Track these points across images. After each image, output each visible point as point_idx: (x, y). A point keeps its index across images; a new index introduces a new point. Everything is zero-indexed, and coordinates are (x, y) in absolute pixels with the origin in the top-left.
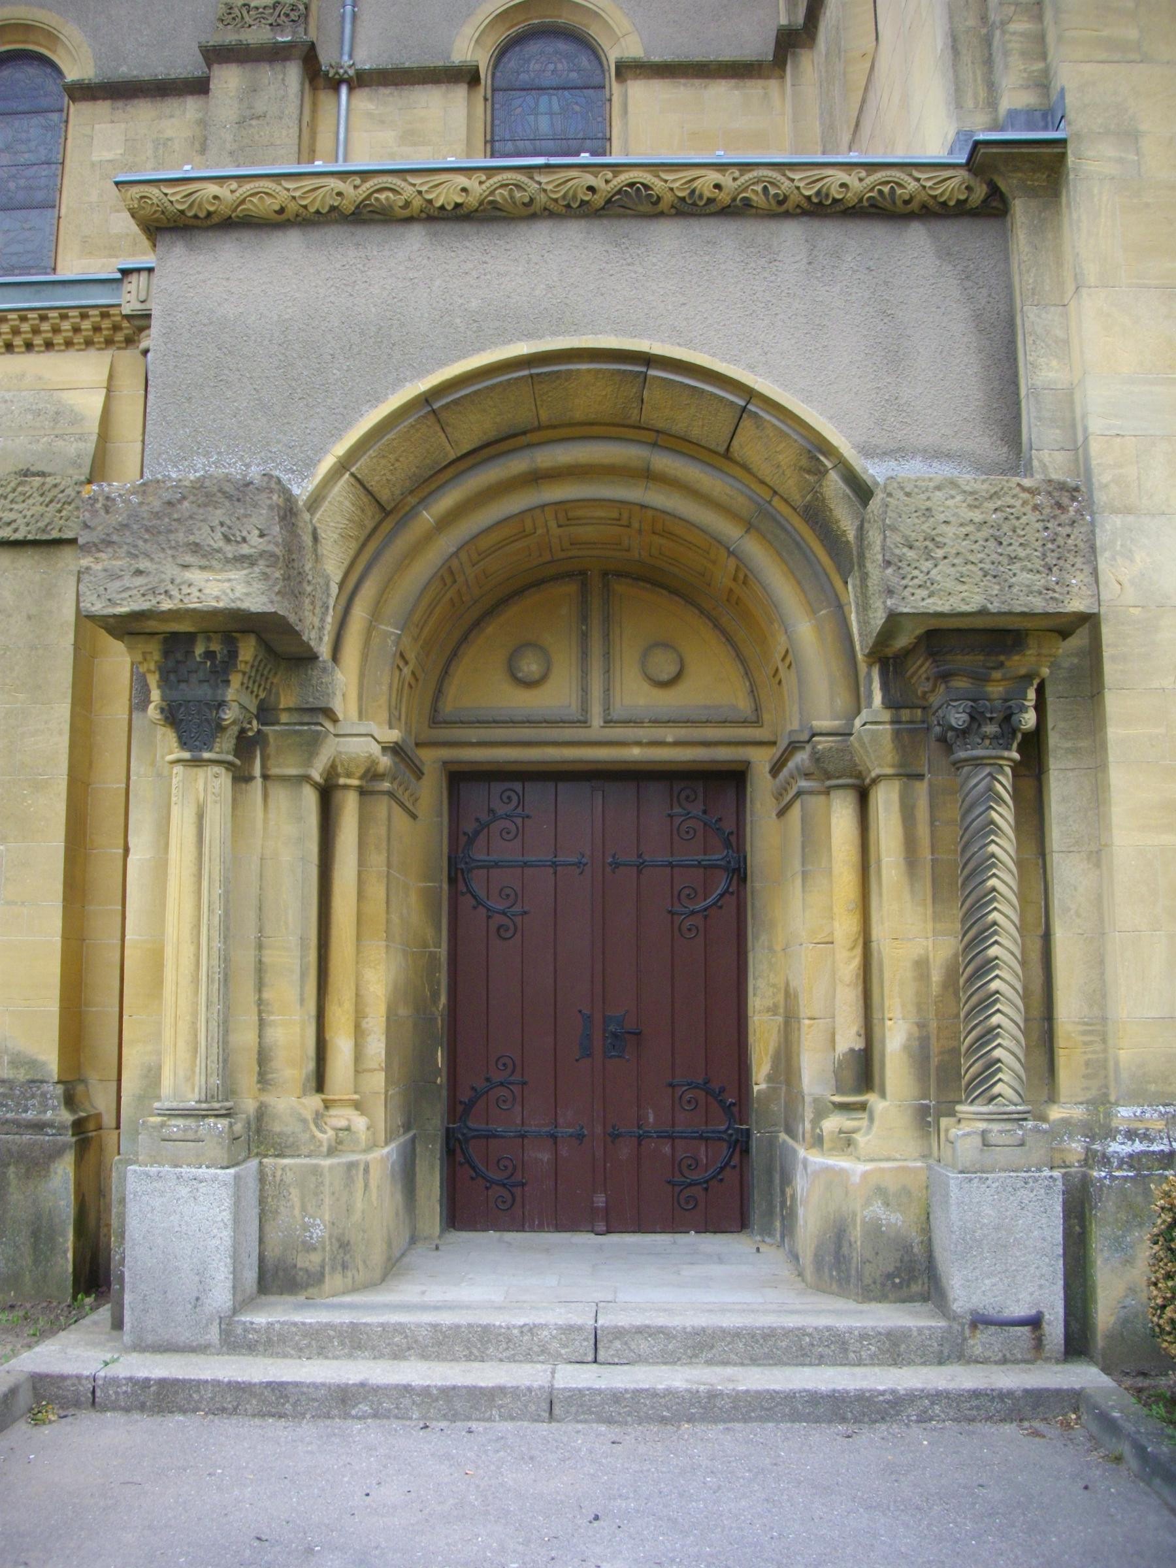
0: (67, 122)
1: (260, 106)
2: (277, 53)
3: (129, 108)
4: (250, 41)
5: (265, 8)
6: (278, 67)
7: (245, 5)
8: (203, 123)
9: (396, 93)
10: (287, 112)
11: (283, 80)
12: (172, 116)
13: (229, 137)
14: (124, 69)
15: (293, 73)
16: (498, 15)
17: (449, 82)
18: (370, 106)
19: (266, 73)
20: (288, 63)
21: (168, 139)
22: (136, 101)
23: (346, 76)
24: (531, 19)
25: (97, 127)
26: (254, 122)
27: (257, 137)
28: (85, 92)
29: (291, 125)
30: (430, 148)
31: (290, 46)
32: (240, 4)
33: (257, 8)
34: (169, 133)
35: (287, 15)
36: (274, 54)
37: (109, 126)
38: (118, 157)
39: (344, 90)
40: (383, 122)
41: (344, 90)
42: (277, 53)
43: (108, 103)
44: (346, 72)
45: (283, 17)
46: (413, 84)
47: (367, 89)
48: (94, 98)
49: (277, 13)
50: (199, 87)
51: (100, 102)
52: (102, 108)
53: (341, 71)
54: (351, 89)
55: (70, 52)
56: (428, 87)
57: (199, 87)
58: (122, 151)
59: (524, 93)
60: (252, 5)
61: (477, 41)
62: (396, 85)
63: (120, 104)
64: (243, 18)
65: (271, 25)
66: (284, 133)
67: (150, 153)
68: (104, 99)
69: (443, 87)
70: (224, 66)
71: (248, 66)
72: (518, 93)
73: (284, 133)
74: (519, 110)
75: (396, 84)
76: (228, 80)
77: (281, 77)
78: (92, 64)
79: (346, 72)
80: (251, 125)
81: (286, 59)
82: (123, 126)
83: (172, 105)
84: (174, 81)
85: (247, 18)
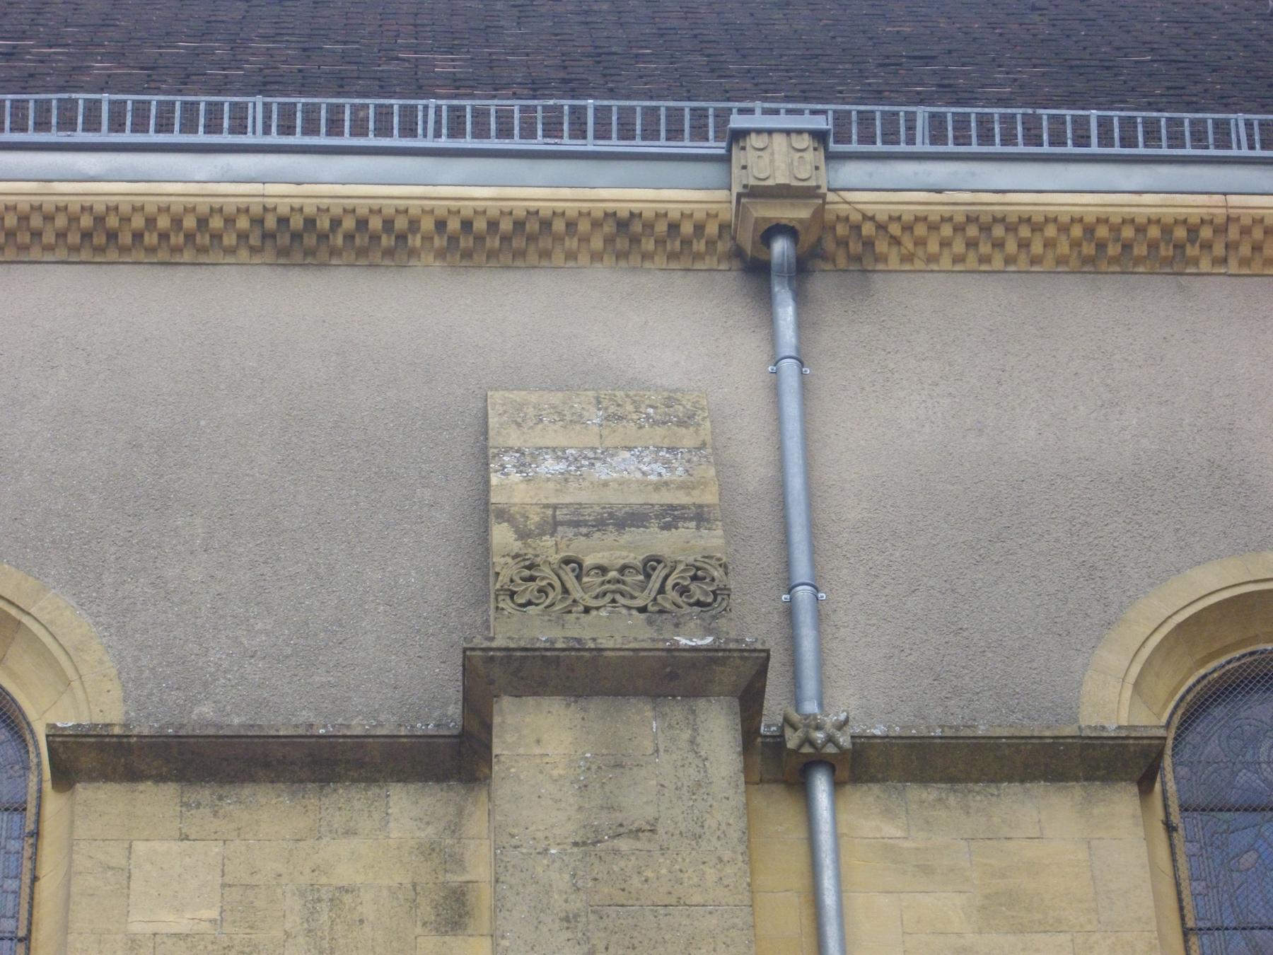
0: (36, 834)
1: (638, 803)
2: (673, 676)
3: (228, 806)
4: (605, 643)
5: (623, 569)
6: (676, 710)
7: (567, 561)
8: (443, 855)
9: (952, 800)
10: (711, 822)
11: (692, 742)
12: (350, 833)
13: (561, 880)
14: (206, 711)
15: (717, 728)
16: (1180, 626)
17: (1090, 778)
18: (891, 830)
19: (644, 725)
20: (702, 703)
21: (342, 889)
22: (247, 791)
23: (831, 749)
24: (1255, 639)
25: (140, 847)
26: (624, 845)
27: (636, 882)
28: (90, 758)
29: (727, 855)
30: (1063, 938)
31: (708, 660)
32: (555, 558)
33: (603, 570)
34: (345, 874)
35: (684, 591)
36: (667, 679)
37: (176, 847)
38: (205, 926)
39: (821, 787)
40: (926, 870)
41: (821, 787)
42: (673, 676)
43: (170, 790)
44: (830, 739)
45: (672, 595)
46: (995, 780)
47: (876, 788)
48: (132, 775)
49: (655, 583)
50: (456, 758)
51: (146, 787)
52: (155, 800)
53: (819, 736)
54: (837, 786)
55: (44, 652)
56: (1038, 788)
57: (456, 758)
58: (214, 913)
59: (1257, 817)
60: (589, 561)
61: (1136, 685)
62: (952, 780)
63: (204, 793)
64: (566, 591)
65: (643, 610)
66: (711, 874)
67: (293, 921)
68: (160, 778)
69: (1077, 790)
70: (531, 701)
71: (596, 706)
72: (1241, 818)
73: (711, 874)
74: (1250, 858)
75: (951, 778)
76: (541, 741)
77: (686, 735)
78: (117, 693)
79: (830, 739)
80: (616, 852)
81: (696, 692)
82: (216, 848)
83: (347, 804)
84: (360, 742)
85: (577, 593)
